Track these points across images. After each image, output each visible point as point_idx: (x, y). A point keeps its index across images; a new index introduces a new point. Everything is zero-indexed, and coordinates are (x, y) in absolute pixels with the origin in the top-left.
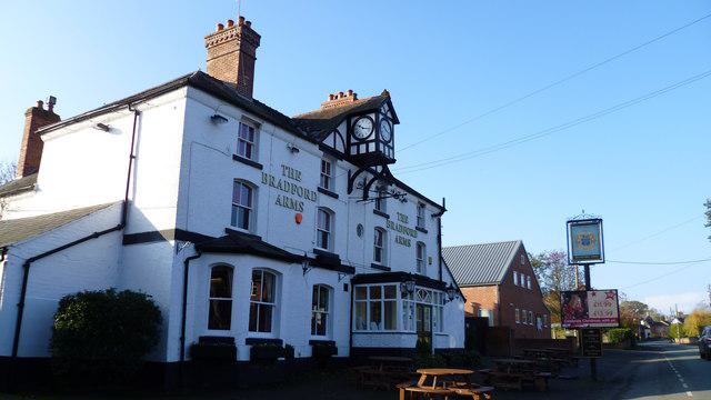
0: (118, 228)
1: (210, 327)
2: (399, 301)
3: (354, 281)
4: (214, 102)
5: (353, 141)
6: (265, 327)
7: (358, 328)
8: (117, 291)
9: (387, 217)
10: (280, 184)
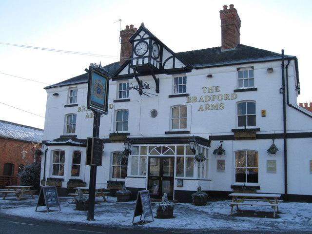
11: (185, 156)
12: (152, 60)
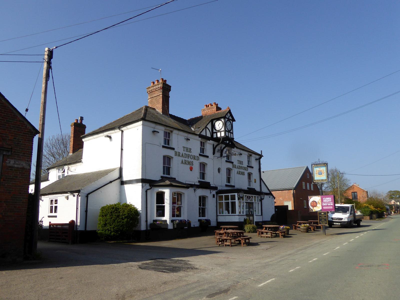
0: (119, 178)
1: (255, 222)
2: (237, 201)
3: (217, 193)
4: (153, 125)
5: (214, 131)
6: (179, 216)
7: (220, 213)
8: (121, 204)
9: (232, 163)
10: (182, 155)
11: (224, 201)
12: (227, 133)
